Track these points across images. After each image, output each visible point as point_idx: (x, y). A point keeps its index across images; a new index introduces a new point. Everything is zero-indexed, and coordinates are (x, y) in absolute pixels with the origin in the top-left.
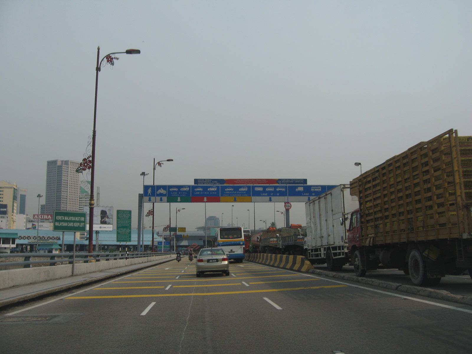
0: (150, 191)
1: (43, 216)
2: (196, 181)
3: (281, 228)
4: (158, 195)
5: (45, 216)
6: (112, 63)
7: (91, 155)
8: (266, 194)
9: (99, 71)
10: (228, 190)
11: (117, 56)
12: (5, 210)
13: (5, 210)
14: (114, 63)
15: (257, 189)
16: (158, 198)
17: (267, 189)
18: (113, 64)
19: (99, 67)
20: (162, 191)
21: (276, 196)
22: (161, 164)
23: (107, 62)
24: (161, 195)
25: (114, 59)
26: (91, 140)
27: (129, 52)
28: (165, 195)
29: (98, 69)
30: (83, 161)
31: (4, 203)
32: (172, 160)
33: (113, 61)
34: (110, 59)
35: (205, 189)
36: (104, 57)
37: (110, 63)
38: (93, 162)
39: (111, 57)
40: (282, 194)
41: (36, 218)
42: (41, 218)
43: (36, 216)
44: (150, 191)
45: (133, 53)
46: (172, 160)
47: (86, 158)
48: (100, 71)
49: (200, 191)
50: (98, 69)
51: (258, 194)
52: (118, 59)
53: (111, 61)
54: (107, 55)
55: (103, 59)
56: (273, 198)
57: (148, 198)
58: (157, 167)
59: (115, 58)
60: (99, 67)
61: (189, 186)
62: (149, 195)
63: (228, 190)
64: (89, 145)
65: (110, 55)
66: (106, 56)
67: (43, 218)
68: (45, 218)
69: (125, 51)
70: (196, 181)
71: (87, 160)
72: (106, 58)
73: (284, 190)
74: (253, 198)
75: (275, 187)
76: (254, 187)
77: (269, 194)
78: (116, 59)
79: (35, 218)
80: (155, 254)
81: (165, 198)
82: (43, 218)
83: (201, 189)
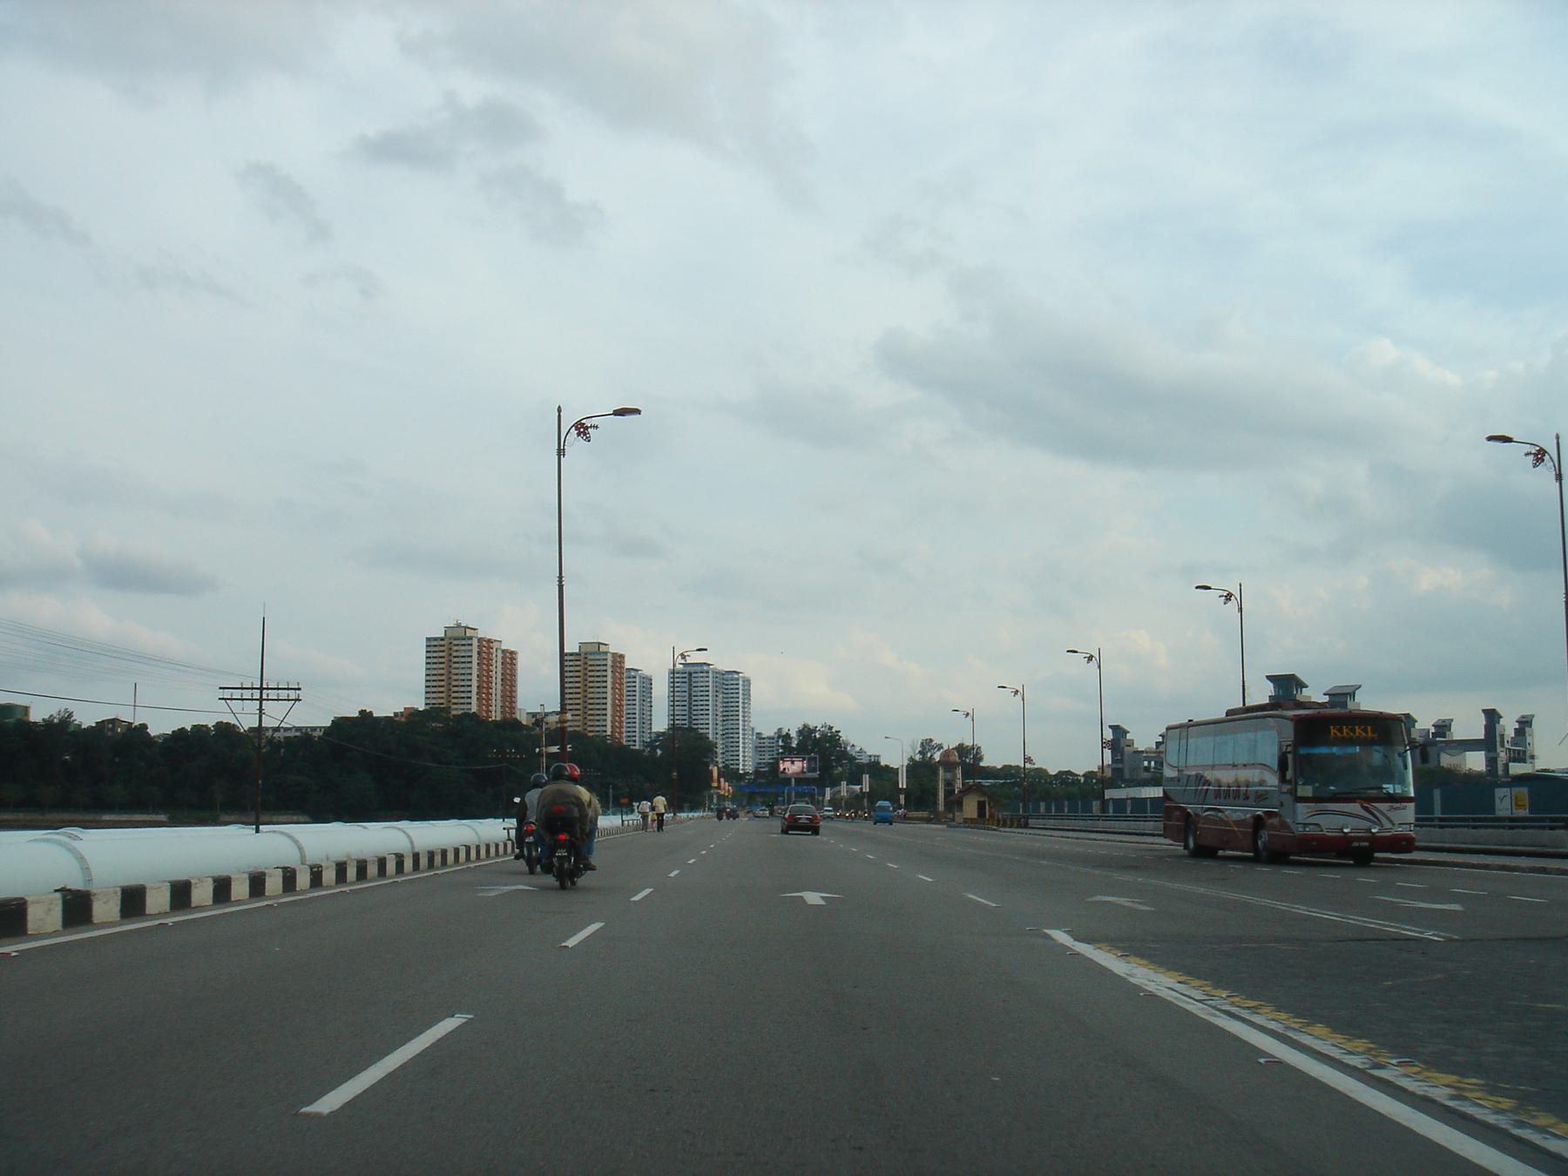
59: (591, 427)
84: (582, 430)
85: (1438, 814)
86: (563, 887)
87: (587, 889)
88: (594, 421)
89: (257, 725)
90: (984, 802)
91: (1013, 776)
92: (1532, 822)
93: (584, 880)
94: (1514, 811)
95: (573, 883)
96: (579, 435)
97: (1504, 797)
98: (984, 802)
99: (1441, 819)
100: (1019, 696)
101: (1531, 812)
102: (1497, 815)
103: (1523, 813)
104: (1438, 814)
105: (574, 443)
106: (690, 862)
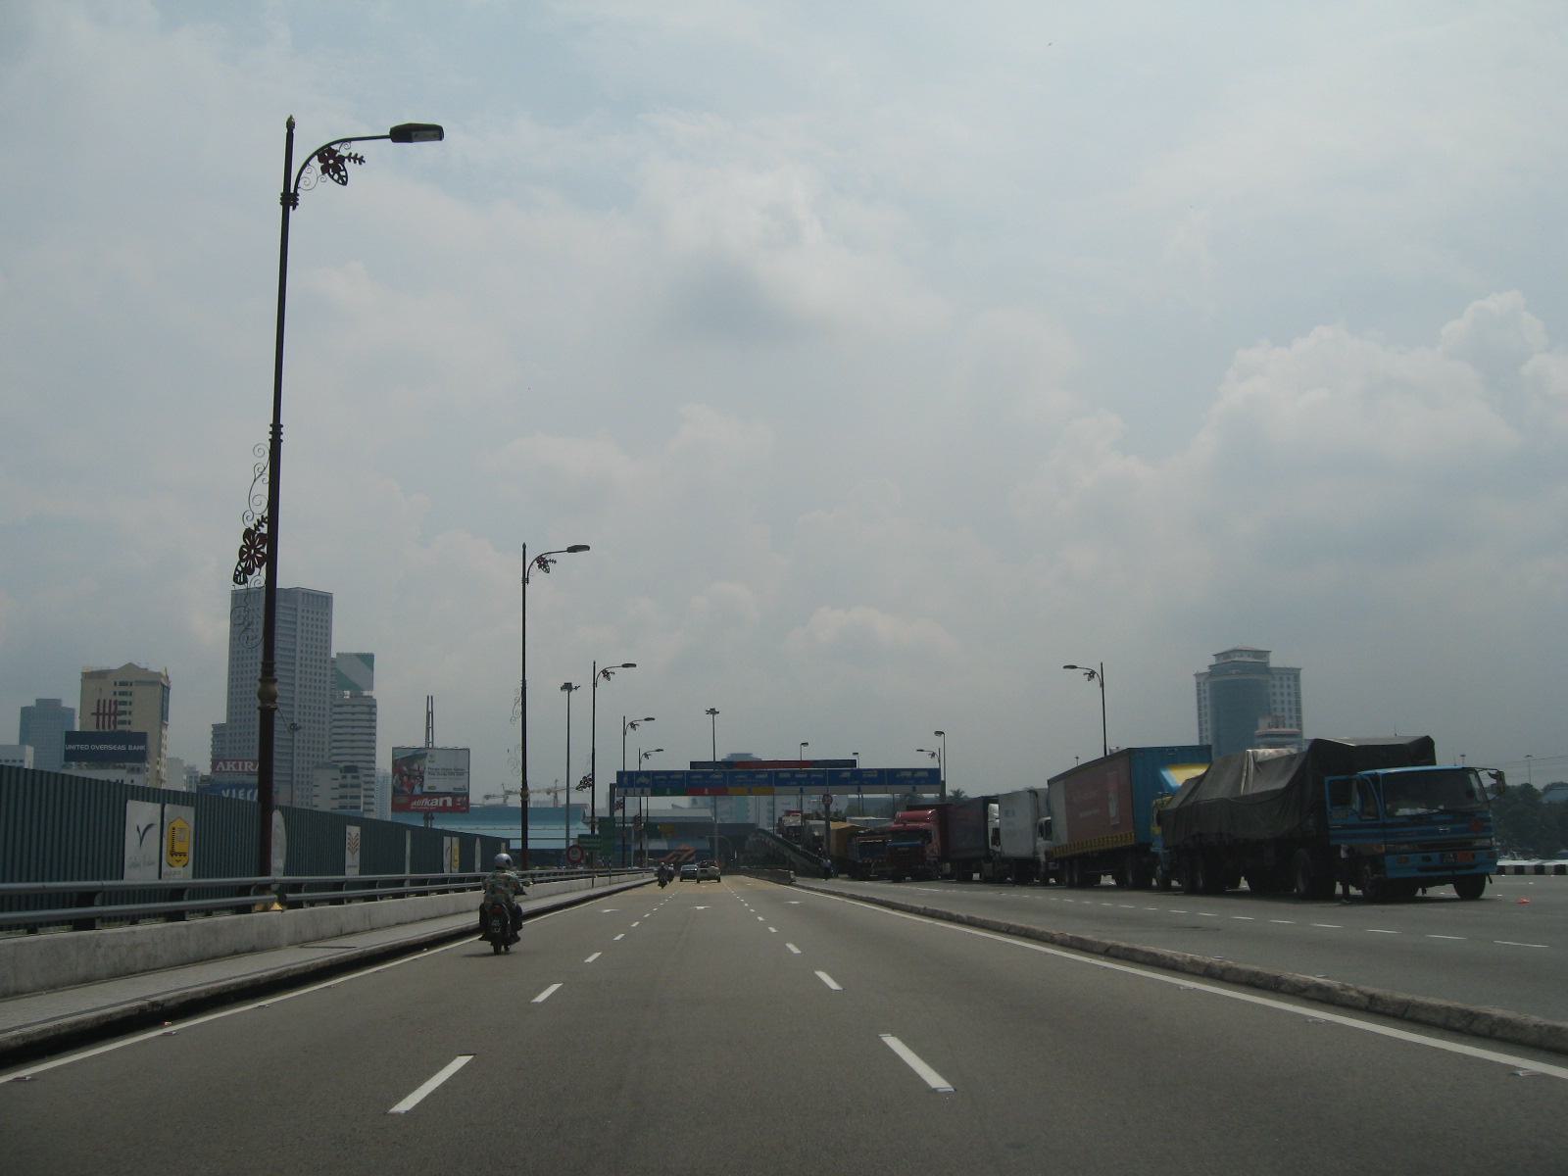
0: (626, 779)
1: (240, 763)
2: (693, 764)
3: (993, 794)
4: (638, 786)
5: (246, 763)
6: (341, 177)
7: (266, 515)
8: (795, 783)
9: (291, 207)
10: (740, 777)
11: (356, 148)
12: (142, 748)
13: (142, 748)
14: (346, 176)
15: (781, 775)
16: (638, 790)
17: (797, 776)
18: (609, 679)
19: (292, 191)
20: (643, 780)
21: (810, 785)
22: (547, 562)
23: (323, 173)
24: (641, 785)
25: (346, 160)
26: (265, 460)
27: (573, 549)
28: (647, 786)
29: (289, 200)
30: (245, 541)
31: (136, 728)
32: (587, 548)
33: (345, 170)
34: (542, 562)
35: (706, 775)
36: (311, 153)
37: (332, 177)
38: (593, 779)
39: (336, 151)
40: (819, 782)
41: (221, 769)
42: (234, 769)
43: (221, 763)
44: (626, 779)
45: (416, 135)
46: (587, 548)
47: (253, 528)
48: (294, 208)
49: (698, 779)
50: (289, 200)
51: (784, 782)
52: (361, 160)
53: (337, 170)
54: (322, 148)
55: (307, 163)
56: (805, 788)
57: (622, 790)
58: (629, 730)
59: (349, 157)
60: (292, 191)
61: (683, 772)
62: (625, 786)
63: (740, 777)
64: (259, 480)
65: (335, 147)
66: (318, 151)
67: (240, 769)
68: (246, 769)
69: (388, 134)
70: (693, 764)
71: (254, 533)
72: (316, 157)
73: (820, 776)
74: (777, 789)
75: (809, 772)
76: (777, 773)
77: (799, 782)
78: (355, 162)
79: (217, 769)
80: (597, 872)
81: (647, 790)
82: (240, 769)
83: (700, 777)
84: (331, 162)
85: (352, 873)
86: (497, 952)
87: (515, 953)
88: (356, 148)
89: (1102, 755)
90: (994, 843)
91: (191, 782)
92: (218, 896)
93: (513, 948)
94: (165, 868)
95: (507, 949)
96: (324, 170)
97: (149, 826)
98: (994, 843)
99: (414, 882)
100: (1096, 681)
101: (361, 873)
102: (125, 882)
103: (180, 874)
104: (352, 873)
105: (315, 185)
106: (637, 923)
